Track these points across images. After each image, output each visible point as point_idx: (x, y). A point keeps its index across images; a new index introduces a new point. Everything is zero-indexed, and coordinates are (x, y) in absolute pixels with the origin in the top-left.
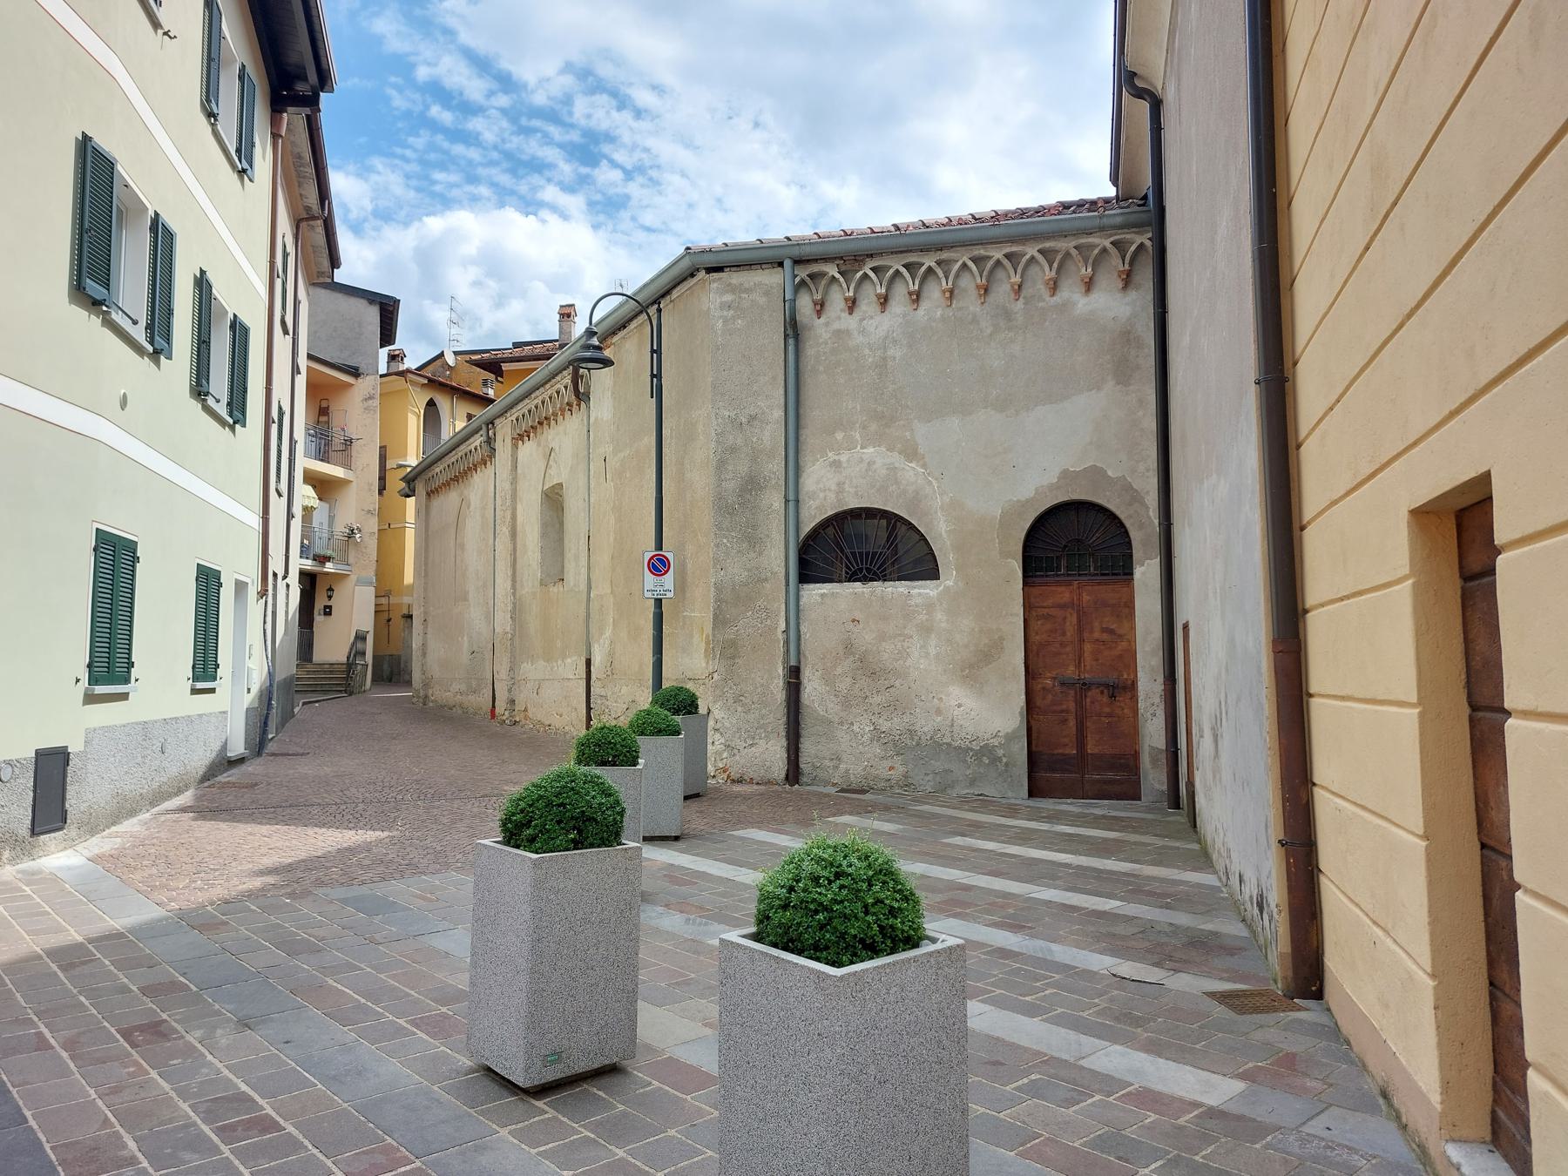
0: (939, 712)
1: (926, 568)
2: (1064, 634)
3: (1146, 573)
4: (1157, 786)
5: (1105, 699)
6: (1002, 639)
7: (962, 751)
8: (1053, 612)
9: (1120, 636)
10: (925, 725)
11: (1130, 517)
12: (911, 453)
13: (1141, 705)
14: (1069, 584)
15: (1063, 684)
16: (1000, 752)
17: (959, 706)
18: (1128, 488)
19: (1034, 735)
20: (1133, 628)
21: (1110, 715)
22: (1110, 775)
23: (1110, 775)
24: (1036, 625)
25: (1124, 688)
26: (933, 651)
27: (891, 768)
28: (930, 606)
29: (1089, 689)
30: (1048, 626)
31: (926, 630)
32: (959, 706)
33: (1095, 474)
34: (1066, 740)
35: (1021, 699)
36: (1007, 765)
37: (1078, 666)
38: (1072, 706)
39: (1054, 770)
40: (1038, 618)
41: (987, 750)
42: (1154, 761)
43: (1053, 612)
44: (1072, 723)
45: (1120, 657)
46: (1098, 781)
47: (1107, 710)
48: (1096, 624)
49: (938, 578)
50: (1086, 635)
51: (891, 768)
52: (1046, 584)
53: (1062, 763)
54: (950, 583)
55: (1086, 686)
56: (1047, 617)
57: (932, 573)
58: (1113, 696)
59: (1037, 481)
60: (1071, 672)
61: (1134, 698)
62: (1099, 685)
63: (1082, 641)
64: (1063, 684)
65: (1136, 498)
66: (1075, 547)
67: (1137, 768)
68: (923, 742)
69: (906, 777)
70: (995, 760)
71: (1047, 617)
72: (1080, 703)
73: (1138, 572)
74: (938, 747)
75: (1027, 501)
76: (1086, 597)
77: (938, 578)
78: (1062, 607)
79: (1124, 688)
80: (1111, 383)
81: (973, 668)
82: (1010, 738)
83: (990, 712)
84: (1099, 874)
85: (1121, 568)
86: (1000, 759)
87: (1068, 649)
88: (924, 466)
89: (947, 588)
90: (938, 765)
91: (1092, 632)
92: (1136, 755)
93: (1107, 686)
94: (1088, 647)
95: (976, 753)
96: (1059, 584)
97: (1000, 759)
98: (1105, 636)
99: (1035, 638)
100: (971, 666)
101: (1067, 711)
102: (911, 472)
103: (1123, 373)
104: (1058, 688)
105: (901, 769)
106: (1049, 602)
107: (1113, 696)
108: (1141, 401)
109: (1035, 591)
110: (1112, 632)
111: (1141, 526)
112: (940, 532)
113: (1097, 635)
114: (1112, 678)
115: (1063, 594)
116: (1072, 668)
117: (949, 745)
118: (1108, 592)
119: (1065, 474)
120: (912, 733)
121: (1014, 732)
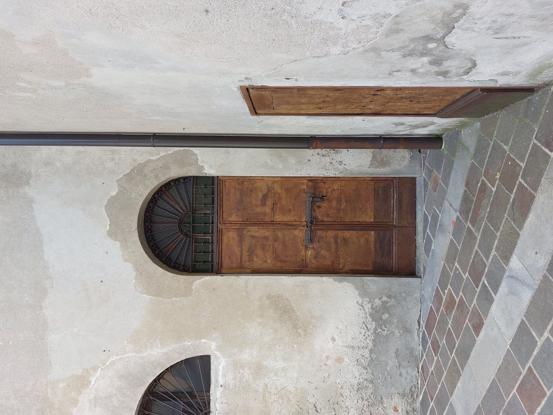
0: (339, 360)
1: (196, 370)
2: (266, 238)
3: (211, 163)
4: (406, 162)
5: (325, 204)
6: (269, 297)
7: (378, 339)
8: (246, 247)
9: (269, 190)
10: (352, 374)
11: (156, 177)
12: (81, 382)
13: (331, 174)
14: (220, 232)
15: (311, 240)
16: (378, 302)
17: (333, 340)
18: (129, 177)
19: (359, 268)
20: (262, 178)
21: (339, 201)
22: (394, 203)
23: (394, 203)
24: (258, 263)
25: (315, 188)
26: (280, 364)
27: (396, 409)
28: (237, 366)
29: (316, 218)
30: (259, 252)
31: (259, 370)
32: (333, 340)
33: (114, 206)
34: (362, 240)
35: (327, 281)
36: (389, 297)
37: (295, 227)
38: (331, 233)
39: (390, 253)
40: (251, 260)
41: (376, 315)
42: (384, 163)
43: (246, 247)
44: (347, 234)
45: (287, 190)
46: (399, 213)
47: (334, 203)
48: (258, 210)
49: (210, 356)
50: (267, 219)
51: (396, 409)
52: (220, 252)
53: (384, 246)
54: (213, 345)
55: (313, 223)
56: (251, 253)
57: (204, 362)
58: (322, 198)
59: (123, 261)
60: (300, 233)
61: (324, 180)
62: (312, 209)
63: (272, 223)
64: (311, 240)
65: (138, 172)
66: (182, 229)
67: (386, 180)
68: (369, 376)
69: (403, 395)
70: (385, 308)
71: (251, 253)
72: (329, 226)
73: (210, 171)
74: (373, 363)
75: (136, 269)
76: (234, 218)
77: (210, 356)
78: (241, 240)
79: (315, 188)
80: (28, 191)
81: (295, 323)
82: (363, 292)
83: (339, 307)
84: (68, 142)
85: (207, 187)
86: (384, 303)
87: (280, 234)
88: (95, 369)
89: (219, 348)
90: (392, 362)
91: (265, 214)
92: (376, 180)
93: (313, 203)
94: (278, 218)
95: (379, 325)
96: (220, 241)
97: (384, 303)
98: (269, 202)
99: (270, 263)
100: (295, 327)
101: (336, 238)
102: (101, 382)
103: (17, 179)
104: (315, 245)
105: (396, 400)
106: (237, 251)
107: (322, 198)
108: (47, 164)
109: (226, 262)
110: (265, 198)
111: (167, 167)
112: (162, 354)
113: (268, 210)
114: (306, 198)
115: (230, 237)
116: (297, 232)
117: (371, 351)
118: (230, 200)
119: (112, 234)
120: (360, 388)
121: (357, 288)
